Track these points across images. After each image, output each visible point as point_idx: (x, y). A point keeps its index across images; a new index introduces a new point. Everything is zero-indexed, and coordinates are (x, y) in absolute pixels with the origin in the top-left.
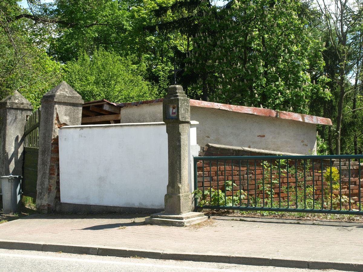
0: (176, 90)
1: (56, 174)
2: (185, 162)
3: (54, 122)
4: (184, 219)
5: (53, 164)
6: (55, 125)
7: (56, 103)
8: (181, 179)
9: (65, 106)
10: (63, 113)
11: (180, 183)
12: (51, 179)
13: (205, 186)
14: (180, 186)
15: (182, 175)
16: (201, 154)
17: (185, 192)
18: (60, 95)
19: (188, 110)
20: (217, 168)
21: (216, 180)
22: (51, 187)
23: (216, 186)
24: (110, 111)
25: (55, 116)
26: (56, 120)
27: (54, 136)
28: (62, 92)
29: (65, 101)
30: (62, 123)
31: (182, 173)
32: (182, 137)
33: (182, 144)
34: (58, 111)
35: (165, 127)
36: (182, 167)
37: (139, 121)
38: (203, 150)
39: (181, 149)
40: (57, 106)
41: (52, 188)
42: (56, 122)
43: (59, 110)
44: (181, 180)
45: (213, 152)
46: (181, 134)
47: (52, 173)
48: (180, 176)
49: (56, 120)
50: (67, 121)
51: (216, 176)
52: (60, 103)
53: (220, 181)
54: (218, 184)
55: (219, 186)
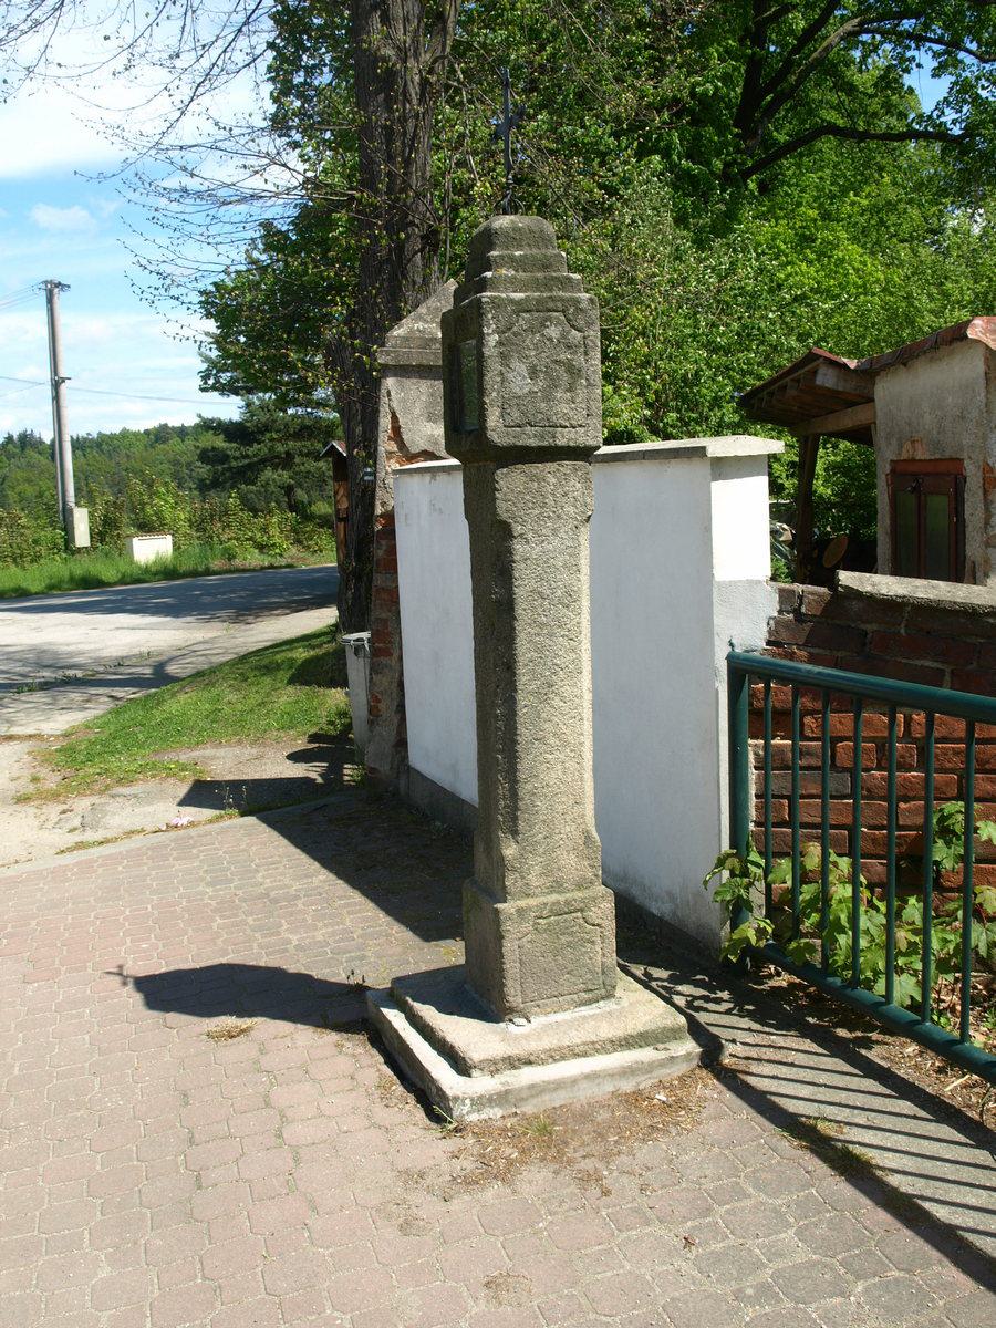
0: (491, 246)
1: (396, 655)
2: (556, 702)
3: (381, 449)
4: (475, 1073)
5: (384, 616)
6: (389, 458)
7: (386, 370)
8: (516, 809)
9: (429, 382)
10: (418, 411)
11: (515, 833)
12: (378, 673)
13: (807, 819)
14: (510, 850)
15: (524, 789)
16: (784, 636)
17: (557, 887)
18: (406, 339)
19: (574, 372)
20: (893, 720)
21: (883, 793)
22: (379, 701)
23: (881, 827)
24: (840, 389)
25: (385, 422)
26: (390, 439)
27: (383, 504)
28: (420, 325)
29: (425, 362)
30: (414, 450)
31: (521, 776)
32: (519, 548)
33: (521, 592)
34: (395, 405)
35: (459, 478)
36: (524, 733)
37: (55, 477)
38: (797, 612)
39: (519, 626)
40: (390, 382)
41: (382, 706)
42: (393, 447)
43: (403, 400)
44: (515, 819)
45: (868, 627)
46: (517, 529)
47: (380, 649)
48: (514, 795)
49: (390, 439)
50: (436, 443)
51: (879, 768)
52: (403, 371)
53: (906, 799)
54: (892, 813)
55: (901, 828)
